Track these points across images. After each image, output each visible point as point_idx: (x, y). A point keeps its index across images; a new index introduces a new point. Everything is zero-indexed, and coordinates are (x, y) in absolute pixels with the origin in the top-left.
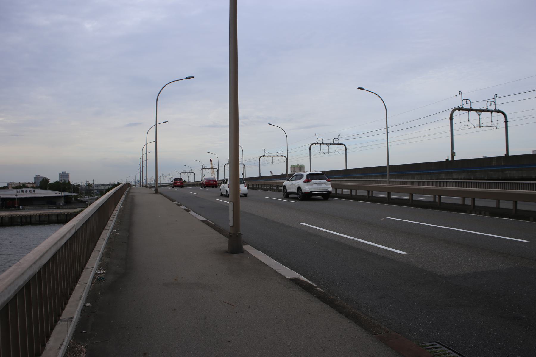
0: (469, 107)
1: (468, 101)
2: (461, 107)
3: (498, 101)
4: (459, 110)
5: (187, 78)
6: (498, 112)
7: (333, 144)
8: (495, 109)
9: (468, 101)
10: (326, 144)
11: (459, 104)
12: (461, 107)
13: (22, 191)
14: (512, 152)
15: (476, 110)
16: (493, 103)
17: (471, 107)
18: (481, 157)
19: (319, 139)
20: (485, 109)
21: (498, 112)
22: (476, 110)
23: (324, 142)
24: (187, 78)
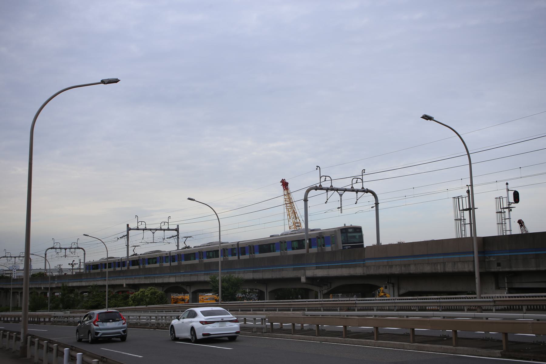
0: (329, 186)
1: (328, 178)
2: (318, 185)
3: (365, 178)
4: (316, 190)
5: (103, 82)
6: (367, 191)
7: (161, 229)
8: (363, 188)
9: (328, 178)
10: (151, 230)
11: (315, 181)
12: (318, 185)
13: (499, 265)
14: (384, 241)
15: (337, 190)
16: (359, 180)
17: (331, 186)
18: (396, 242)
19: (140, 223)
20: (350, 187)
21: (367, 191)
22: (337, 190)
23: (147, 228)
24: (103, 82)
